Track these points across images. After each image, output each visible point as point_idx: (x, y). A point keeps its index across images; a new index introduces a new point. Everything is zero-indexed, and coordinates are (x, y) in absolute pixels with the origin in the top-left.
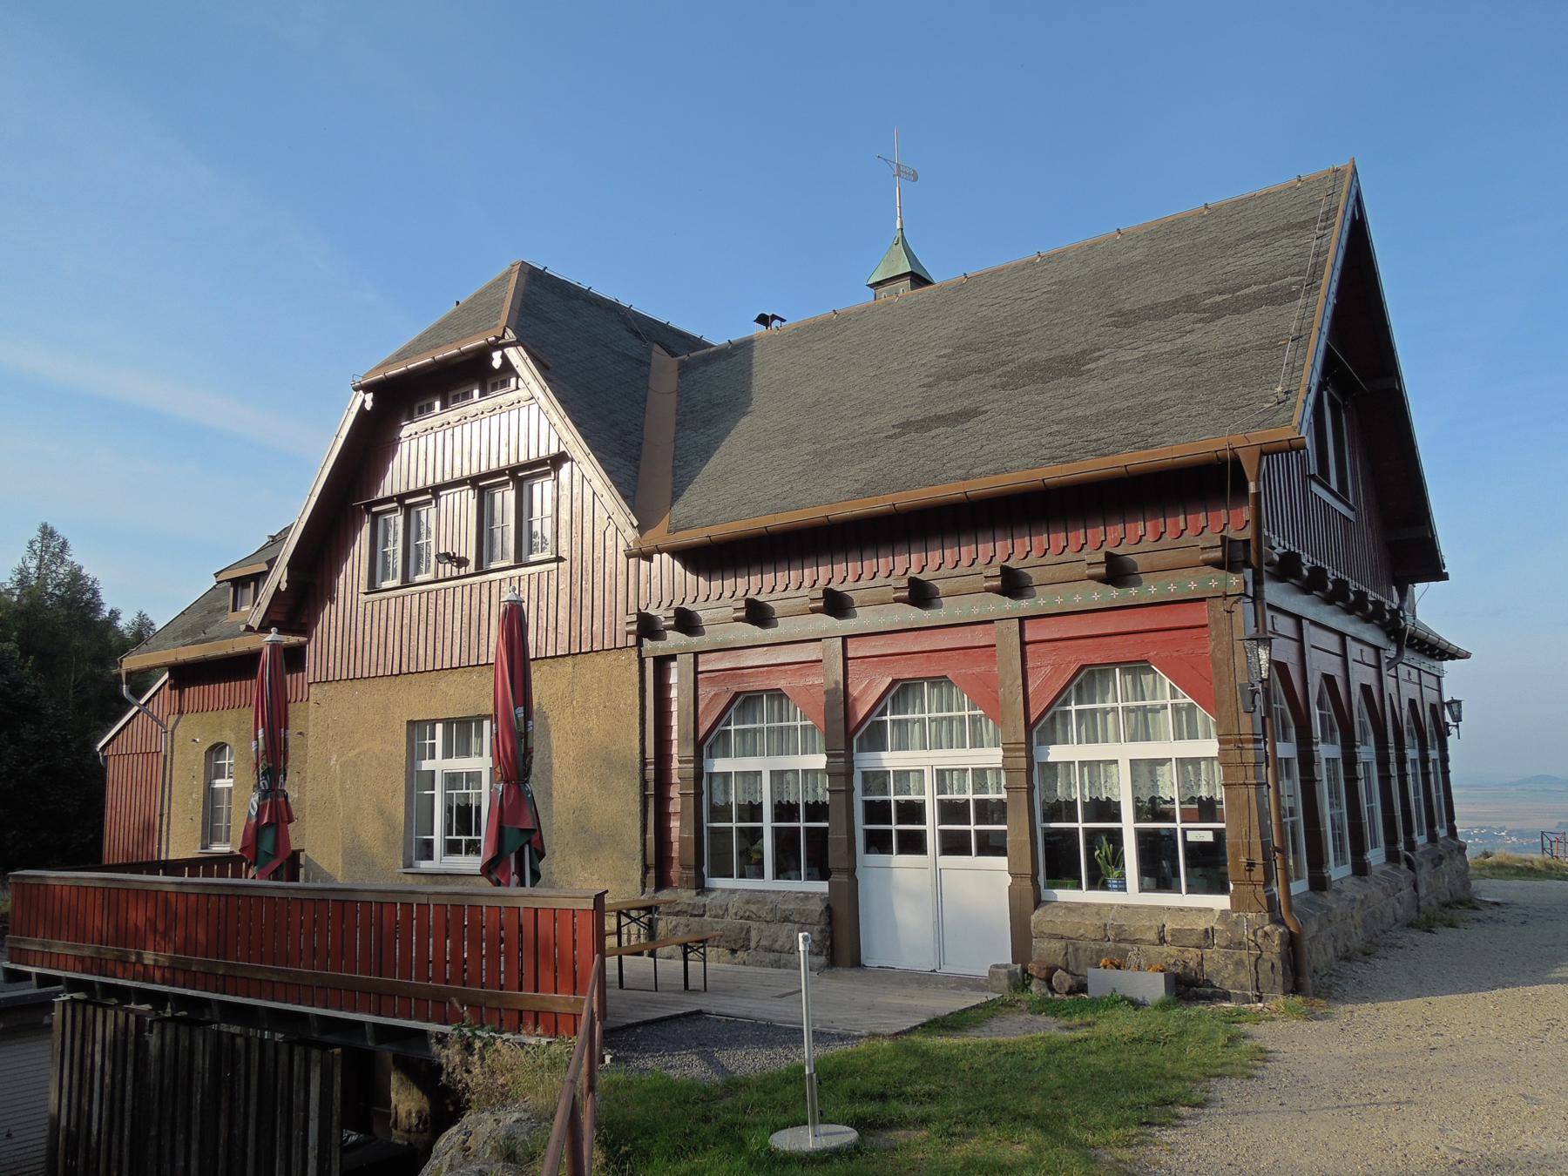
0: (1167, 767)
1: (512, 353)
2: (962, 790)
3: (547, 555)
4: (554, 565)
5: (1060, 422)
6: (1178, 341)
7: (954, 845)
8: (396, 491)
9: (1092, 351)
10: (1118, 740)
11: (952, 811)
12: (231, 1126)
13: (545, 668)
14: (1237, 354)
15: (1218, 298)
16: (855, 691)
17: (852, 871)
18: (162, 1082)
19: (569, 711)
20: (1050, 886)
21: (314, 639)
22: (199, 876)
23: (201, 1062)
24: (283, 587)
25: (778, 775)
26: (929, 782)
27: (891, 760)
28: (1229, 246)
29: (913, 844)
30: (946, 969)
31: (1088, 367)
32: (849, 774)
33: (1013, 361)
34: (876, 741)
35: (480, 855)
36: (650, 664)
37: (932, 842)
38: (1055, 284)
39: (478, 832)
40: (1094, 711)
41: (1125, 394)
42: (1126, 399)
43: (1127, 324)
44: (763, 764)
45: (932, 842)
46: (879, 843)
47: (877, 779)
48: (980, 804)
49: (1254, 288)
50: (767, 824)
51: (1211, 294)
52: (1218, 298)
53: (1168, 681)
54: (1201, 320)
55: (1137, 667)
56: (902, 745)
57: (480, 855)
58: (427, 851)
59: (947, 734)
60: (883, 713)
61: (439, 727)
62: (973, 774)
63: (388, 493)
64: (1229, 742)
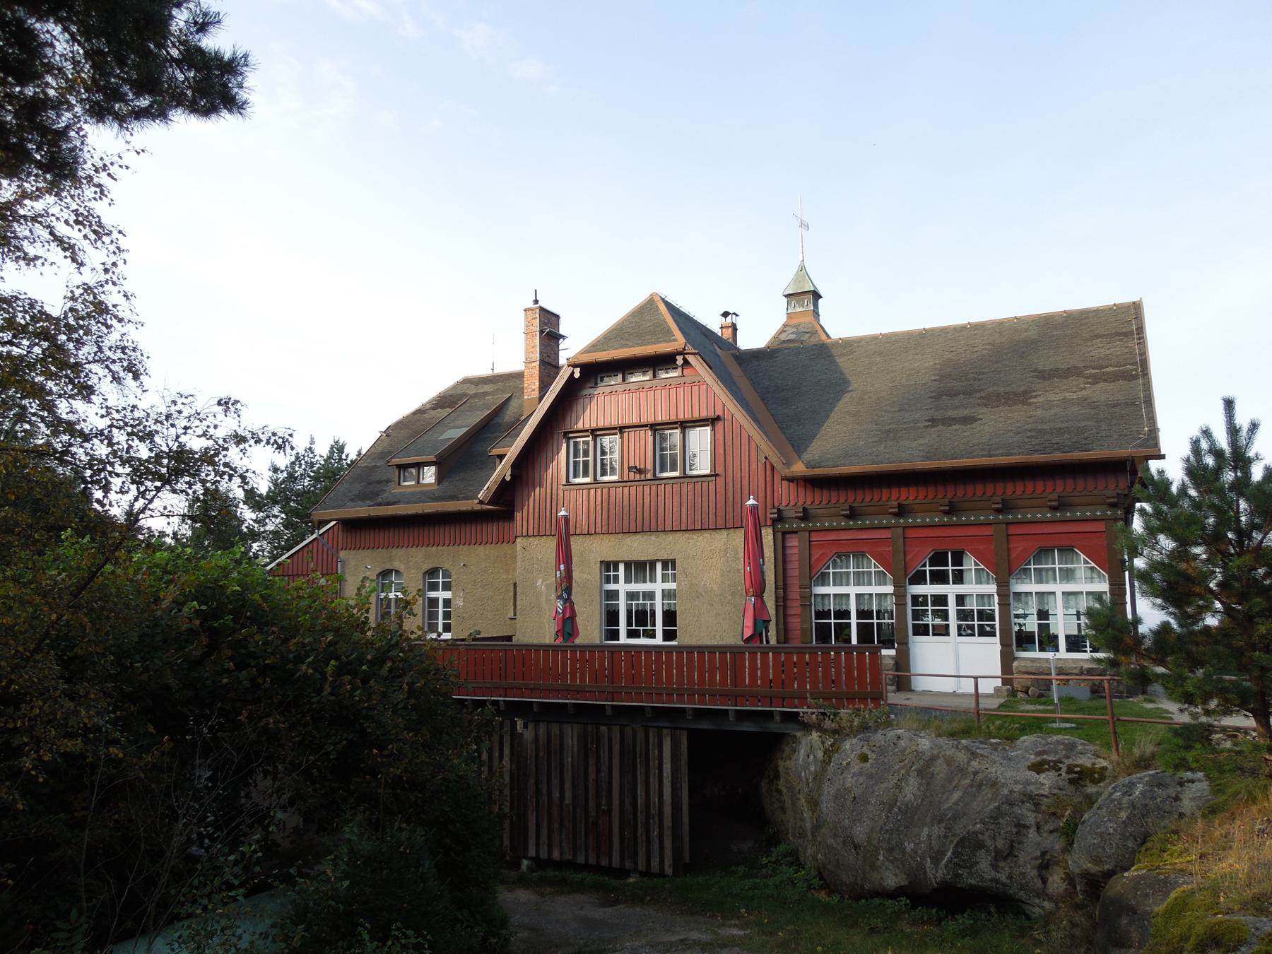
0: (1080, 596)
1: (691, 359)
4: (714, 478)
5: (1030, 431)
6: (1079, 393)
9: (1031, 392)
12: (598, 771)
14: (1115, 406)
15: (1094, 371)
17: (906, 643)
18: (537, 755)
20: (1017, 651)
21: (526, 507)
22: (913, 620)
23: (570, 741)
24: (508, 478)
25: (858, 596)
28: (1086, 340)
30: (961, 691)
31: (1032, 400)
32: (904, 596)
33: (982, 390)
35: (664, 640)
36: (780, 535)
37: (953, 629)
38: (987, 344)
39: (654, 625)
41: (1062, 419)
42: (1063, 422)
43: (1044, 378)
44: (852, 590)
45: (953, 629)
46: (922, 630)
49: (1111, 369)
50: (854, 621)
52: (1094, 371)
53: (1083, 556)
54: (1087, 383)
57: (664, 640)
58: (614, 635)
61: (622, 567)
62: (834, 599)
64: (1115, 585)
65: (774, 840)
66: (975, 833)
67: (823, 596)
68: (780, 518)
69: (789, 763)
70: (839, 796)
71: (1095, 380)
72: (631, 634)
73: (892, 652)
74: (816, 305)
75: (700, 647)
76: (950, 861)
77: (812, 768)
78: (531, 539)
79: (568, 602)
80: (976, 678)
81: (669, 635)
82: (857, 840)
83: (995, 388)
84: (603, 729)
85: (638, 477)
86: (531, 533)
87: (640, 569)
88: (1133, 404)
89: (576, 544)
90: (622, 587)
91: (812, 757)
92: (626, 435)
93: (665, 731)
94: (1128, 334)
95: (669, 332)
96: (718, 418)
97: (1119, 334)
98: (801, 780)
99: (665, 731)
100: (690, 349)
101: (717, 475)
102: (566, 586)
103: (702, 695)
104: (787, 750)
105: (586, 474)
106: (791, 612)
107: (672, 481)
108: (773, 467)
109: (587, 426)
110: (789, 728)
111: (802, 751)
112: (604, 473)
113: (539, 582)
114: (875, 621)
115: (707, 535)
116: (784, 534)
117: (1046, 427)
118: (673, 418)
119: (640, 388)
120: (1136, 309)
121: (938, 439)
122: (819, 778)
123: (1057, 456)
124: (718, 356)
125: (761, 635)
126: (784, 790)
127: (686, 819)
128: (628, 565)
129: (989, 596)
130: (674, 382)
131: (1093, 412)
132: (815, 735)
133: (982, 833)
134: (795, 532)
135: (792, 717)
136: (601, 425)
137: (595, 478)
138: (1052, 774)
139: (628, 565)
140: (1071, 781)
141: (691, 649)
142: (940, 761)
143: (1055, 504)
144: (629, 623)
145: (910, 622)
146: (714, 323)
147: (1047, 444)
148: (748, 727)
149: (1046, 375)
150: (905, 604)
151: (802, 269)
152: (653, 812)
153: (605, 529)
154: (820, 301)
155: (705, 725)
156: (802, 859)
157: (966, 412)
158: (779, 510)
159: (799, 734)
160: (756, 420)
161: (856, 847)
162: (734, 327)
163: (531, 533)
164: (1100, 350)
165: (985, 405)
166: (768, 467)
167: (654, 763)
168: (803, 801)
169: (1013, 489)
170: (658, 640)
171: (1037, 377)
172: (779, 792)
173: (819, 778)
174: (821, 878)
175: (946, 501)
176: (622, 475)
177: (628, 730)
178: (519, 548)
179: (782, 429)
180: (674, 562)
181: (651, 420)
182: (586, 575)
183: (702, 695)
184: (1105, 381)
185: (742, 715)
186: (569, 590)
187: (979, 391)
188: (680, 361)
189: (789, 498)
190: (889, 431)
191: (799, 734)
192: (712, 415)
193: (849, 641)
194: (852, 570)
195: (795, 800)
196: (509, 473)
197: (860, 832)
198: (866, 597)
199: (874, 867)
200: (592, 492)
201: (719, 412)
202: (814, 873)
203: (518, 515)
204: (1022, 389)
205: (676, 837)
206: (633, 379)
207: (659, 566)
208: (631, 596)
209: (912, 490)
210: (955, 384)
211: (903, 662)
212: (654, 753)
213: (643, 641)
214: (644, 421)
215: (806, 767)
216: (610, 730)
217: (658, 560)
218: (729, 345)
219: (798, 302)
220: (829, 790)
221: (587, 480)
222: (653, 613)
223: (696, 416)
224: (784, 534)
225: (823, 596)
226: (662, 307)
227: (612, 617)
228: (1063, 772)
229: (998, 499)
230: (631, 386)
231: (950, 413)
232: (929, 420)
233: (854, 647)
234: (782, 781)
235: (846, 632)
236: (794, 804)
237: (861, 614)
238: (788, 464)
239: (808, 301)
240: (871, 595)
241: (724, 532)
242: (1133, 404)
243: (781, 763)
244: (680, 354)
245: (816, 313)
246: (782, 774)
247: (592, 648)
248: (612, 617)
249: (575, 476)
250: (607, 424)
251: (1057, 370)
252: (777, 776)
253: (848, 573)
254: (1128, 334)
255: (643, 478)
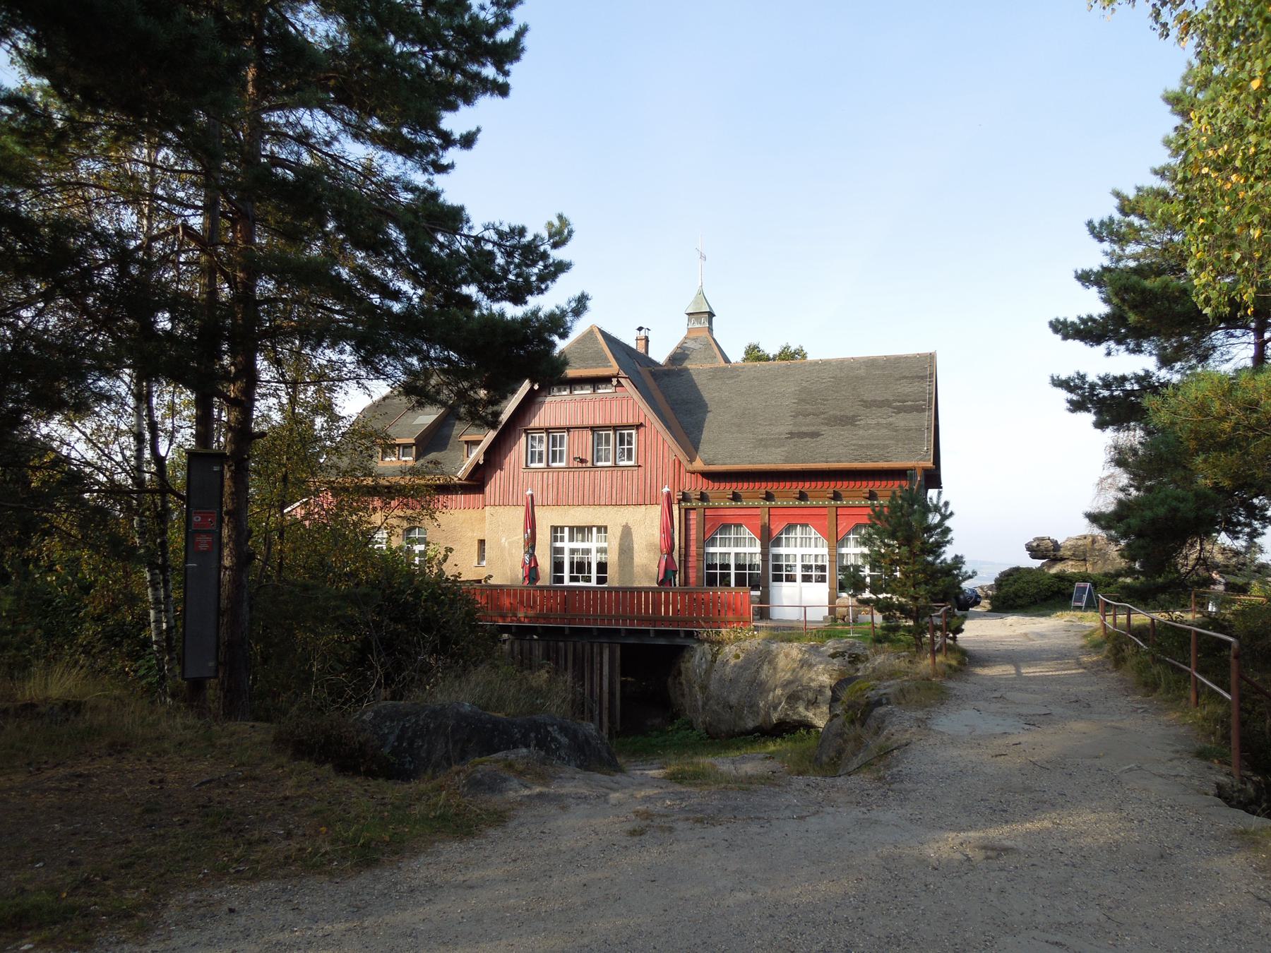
1: (622, 381)
2: (809, 561)
3: (609, 464)
7: (806, 579)
8: (547, 425)
10: (796, 546)
11: (807, 568)
13: (591, 509)
15: (899, 404)
16: (772, 527)
19: (643, 526)
24: (481, 462)
25: (737, 554)
26: (799, 558)
27: (782, 550)
28: (897, 380)
29: (790, 579)
32: (768, 555)
34: (778, 543)
35: (825, 582)
36: (683, 511)
37: (799, 578)
39: (590, 572)
40: (726, 538)
43: (867, 407)
44: (733, 550)
45: (799, 578)
46: (778, 578)
47: (777, 557)
48: (816, 566)
49: (910, 403)
50: (733, 571)
51: (895, 401)
52: (899, 404)
53: (748, 530)
54: (894, 412)
55: (804, 525)
56: (788, 545)
57: (825, 582)
58: (561, 580)
59: (805, 542)
60: (782, 534)
61: (566, 530)
63: (537, 425)
65: (676, 716)
66: (797, 691)
67: (713, 554)
68: (685, 498)
69: (689, 665)
70: (721, 680)
71: (899, 410)
72: (573, 579)
73: (758, 593)
74: (710, 323)
75: (631, 588)
76: (783, 707)
77: (704, 667)
78: (497, 508)
79: (532, 556)
80: (805, 607)
81: (601, 580)
82: (731, 703)
83: (835, 412)
84: (561, 644)
85: (580, 465)
86: (497, 503)
87: (581, 531)
88: (920, 430)
89: (539, 512)
90: (567, 545)
91: (704, 659)
92: (571, 433)
93: (605, 645)
94: (923, 378)
95: (606, 359)
96: (641, 425)
97: (918, 377)
98: (696, 675)
99: (605, 645)
100: (622, 374)
101: (640, 466)
102: (531, 543)
103: (632, 620)
104: (687, 656)
105: (540, 460)
106: (690, 565)
107: (606, 469)
108: (680, 462)
109: (542, 425)
110: (689, 642)
111: (697, 657)
112: (554, 460)
113: (503, 540)
114: (747, 572)
115: (631, 508)
116: (687, 510)
117: (864, 443)
118: (608, 423)
119: (583, 400)
120: (930, 359)
121: (793, 448)
122: (708, 672)
123: (869, 465)
124: (638, 372)
125: (671, 580)
126: (684, 682)
127: (618, 702)
128: (571, 529)
129: (823, 555)
130: (609, 396)
131: (895, 433)
132: (706, 645)
133: (801, 691)
134: (694, 509)
135: (690, 634)
136: (553, 425)
137: (548, 465)
138: (841, 658)
139: (571, 529)
140: (849, 662)
141: (617, 590)
142: (782, 655)
143: (868, 495)
144: (572, 572)
145: (771, 572)
146: (629, 339)
147: (863, 455)
148: (662, 642)
149: (867, 404)
150: (768, 560)
151: (701, 293)
152: (595, 698)
153: (554, 502)
154: (714, 318)
155: (631, 641)
156: (695, 726)
157: (812, 429)
158: (683, 493)
159: (695, 646)
160: (669, 427)
161: (731, 708)
162: (647, 340)
163: (497, 503)
164: (906, 388)
165: (827, 424)
166: (676, 462)
167: (597, 666)
168: (697, 688)
169: (841, 486)
170: (593, 583)
171: (862, 405)
172: (681, 684)
173: (708, 672)
174: (708, 734)
175: (798, 490)
176: (568, 462)
177: (579, 646)
178: (487, 514)
179: (686, 433)
180: (606, 528)
181: (591, 423)
182: (543, 536)
183: (632, 620)
184: (905, 412)
185: (659, 633)
186: (533, 547)
187: (823, 413)
188: (614, 381)
189: (694, 486)
190: (761, 440)
191: (695, 646)
192: (636, 422)
193: (729, 585)
194: (732, 536)
195: (691, 687)
196: (482, 458)
197: (733, 699)
198: (742, 555)
199: (741, 718)
200: (545, 474)
201: (642, 420)
202: (702, 731)
203: (487, 489)
204: (852, 413)
205: (611, 716)
206: (576, 392)
207: (595, 530)
208: (573, 551)
209: (776, 484)
210: (808, 406)
211: (765, 598)
212: (596, 659)
213: (581, 584)
214: (585, 424)
215: (700, 666)
216: (566, 646)
217: (594, 526)
218: (644, 360)
219: (696, 319)
220: (715, 676)
221: (543, 465)
222: (589, 564)
223: (625, 422)
224: (687, 510)
225: (713, 554)
226: (600, 337)
227: (558, 566)
228: (846, 658)
229: (832, 491)
230: (576, 397)
231: (804, 429)
232: (789, 433)
233: (732, 588)
234: (683, 676)
235: (728, 579)
236: (690, 691)
237: (738, 567)
238: (692, 461)
239: (704, 319)
240: (745, 554)
241: (643, 507)
242: (920, 430)
243: (682, 665)
244: (615, 377)
245: (710, 329)
246: (683, 672)
247: (548, 588)
248: (558, 566)
249: (531, 462)
250: (558, 425)
251: (875, 401)
252: (680, 673)
253: (730, 539)
254: (923, 378)
255: (584, 465)
